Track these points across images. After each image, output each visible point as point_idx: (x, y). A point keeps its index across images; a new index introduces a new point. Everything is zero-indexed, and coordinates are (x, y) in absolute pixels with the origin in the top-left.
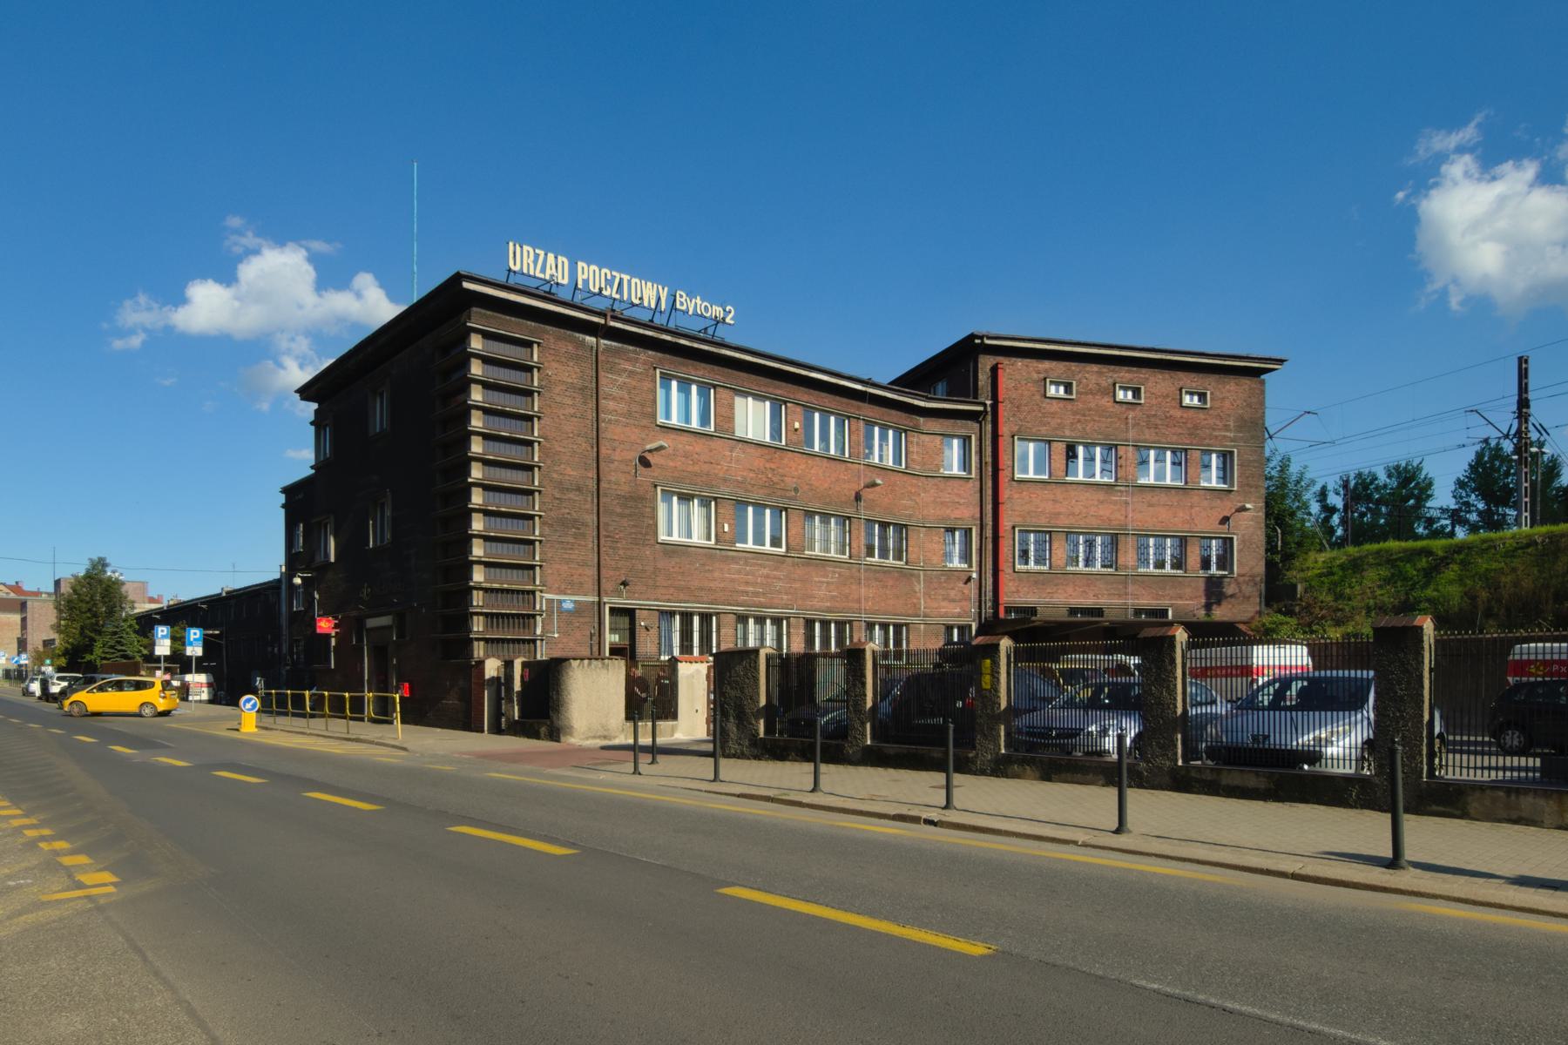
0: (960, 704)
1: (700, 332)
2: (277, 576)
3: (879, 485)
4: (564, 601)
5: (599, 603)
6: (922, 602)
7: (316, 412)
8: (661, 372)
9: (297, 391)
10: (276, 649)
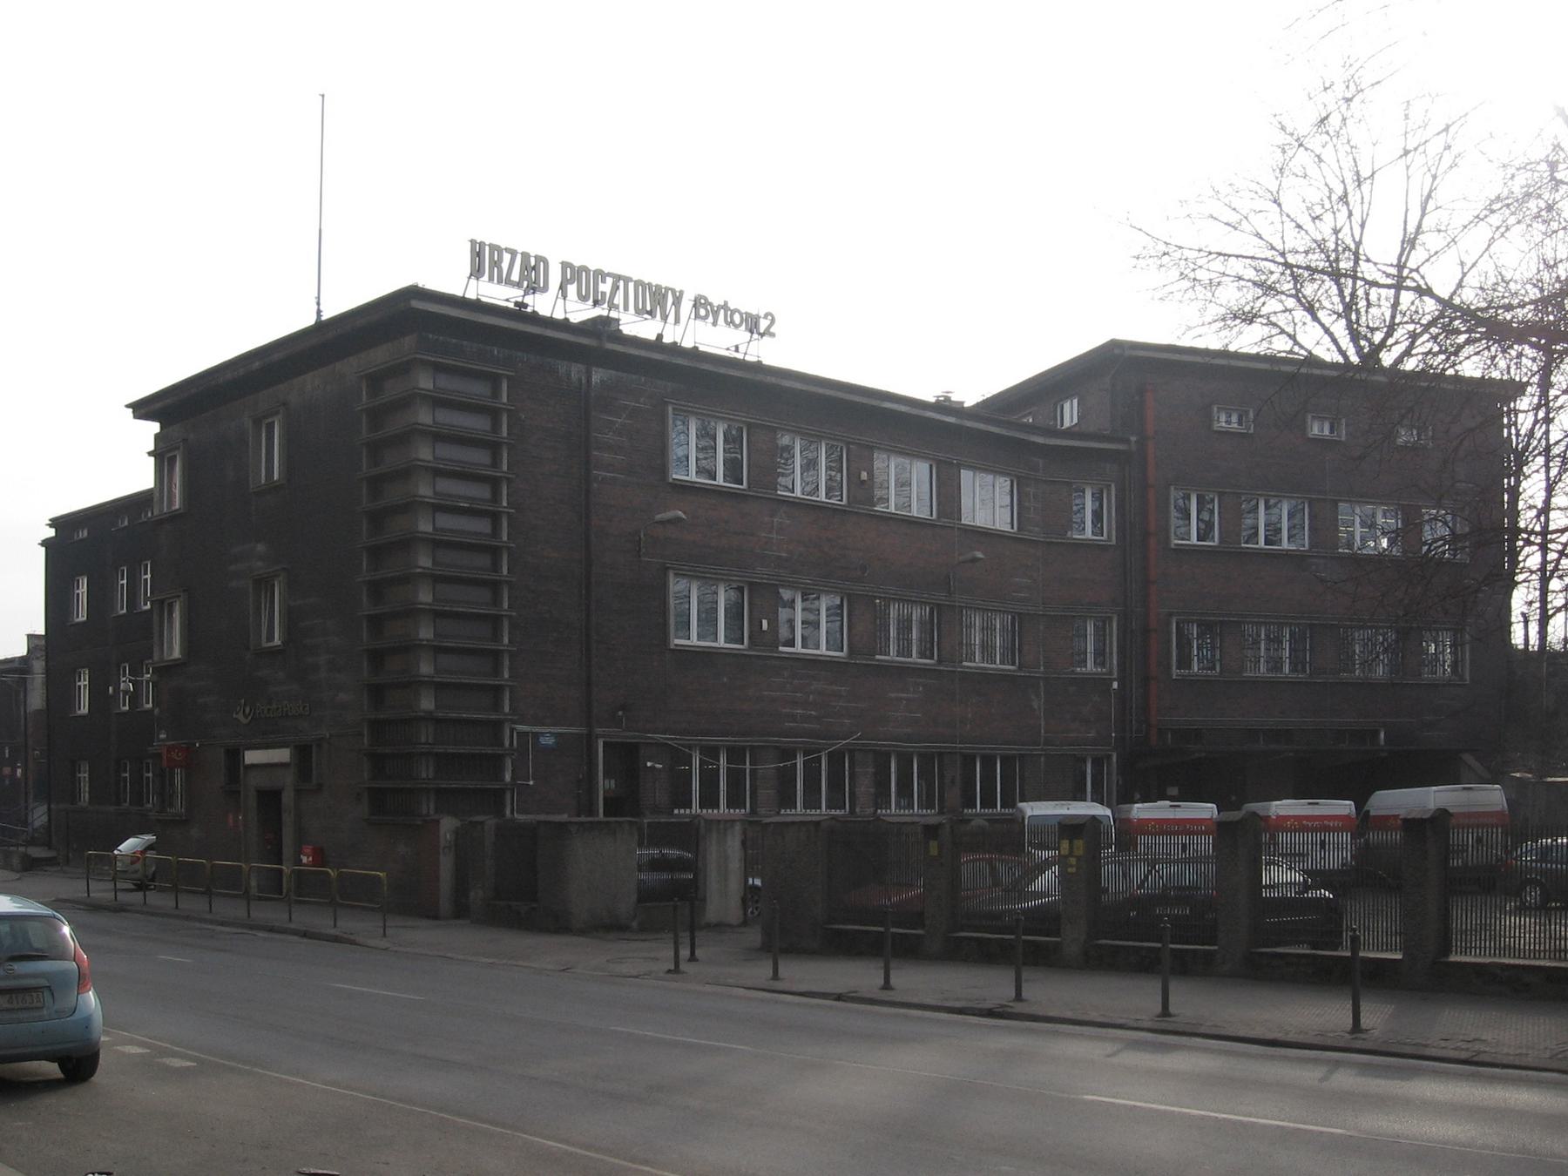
0: (1506, 537)
1: (728, 349)
2: (21, 650)
3: (980, 559)
4: (543, 734)
5: (589, 735)
6: (1043, 723)
7: (157, 437)
8: (674, 409)
9: (143, 409)
10: (19, 771)
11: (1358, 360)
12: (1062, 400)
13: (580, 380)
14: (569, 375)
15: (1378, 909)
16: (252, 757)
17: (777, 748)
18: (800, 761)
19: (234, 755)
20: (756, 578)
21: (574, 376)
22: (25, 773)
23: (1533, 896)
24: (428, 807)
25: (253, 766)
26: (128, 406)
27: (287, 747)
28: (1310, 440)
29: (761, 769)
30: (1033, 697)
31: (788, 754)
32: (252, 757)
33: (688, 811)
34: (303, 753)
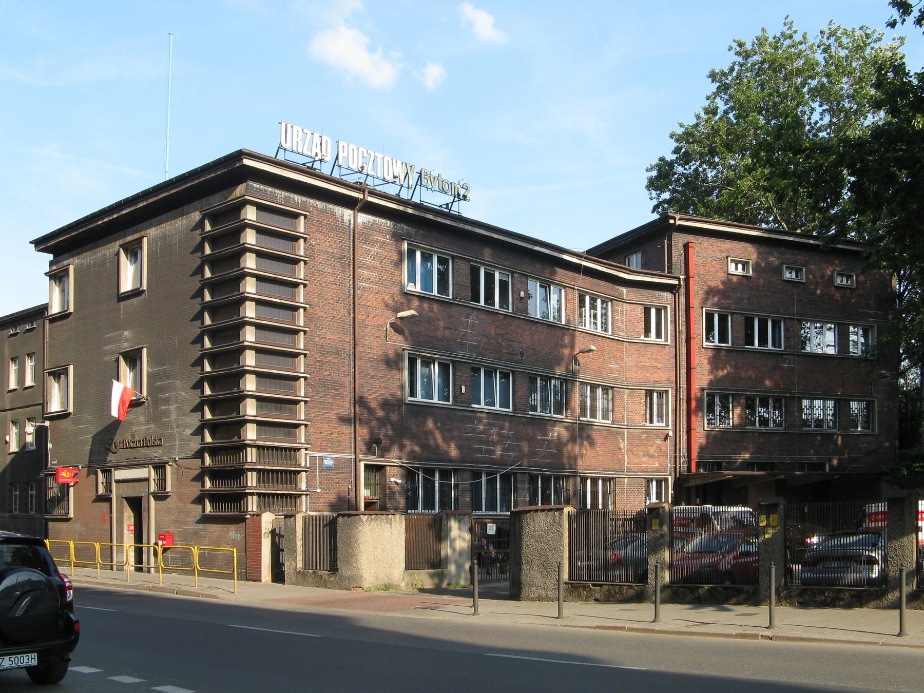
11: (536, 310)
12: (629, 255)
13: (350, 221)
14: (342, 217)
17: (471, 470)
18: (484, 479)
20: (458, 358)
21: (346, 218)
22: (837, 474)
24: (252, 504)
26: (31, 243)
28: (785, 281)
29: (461, 484)
30: (621, 441)
31: (477, 475)
33: (433, 511)
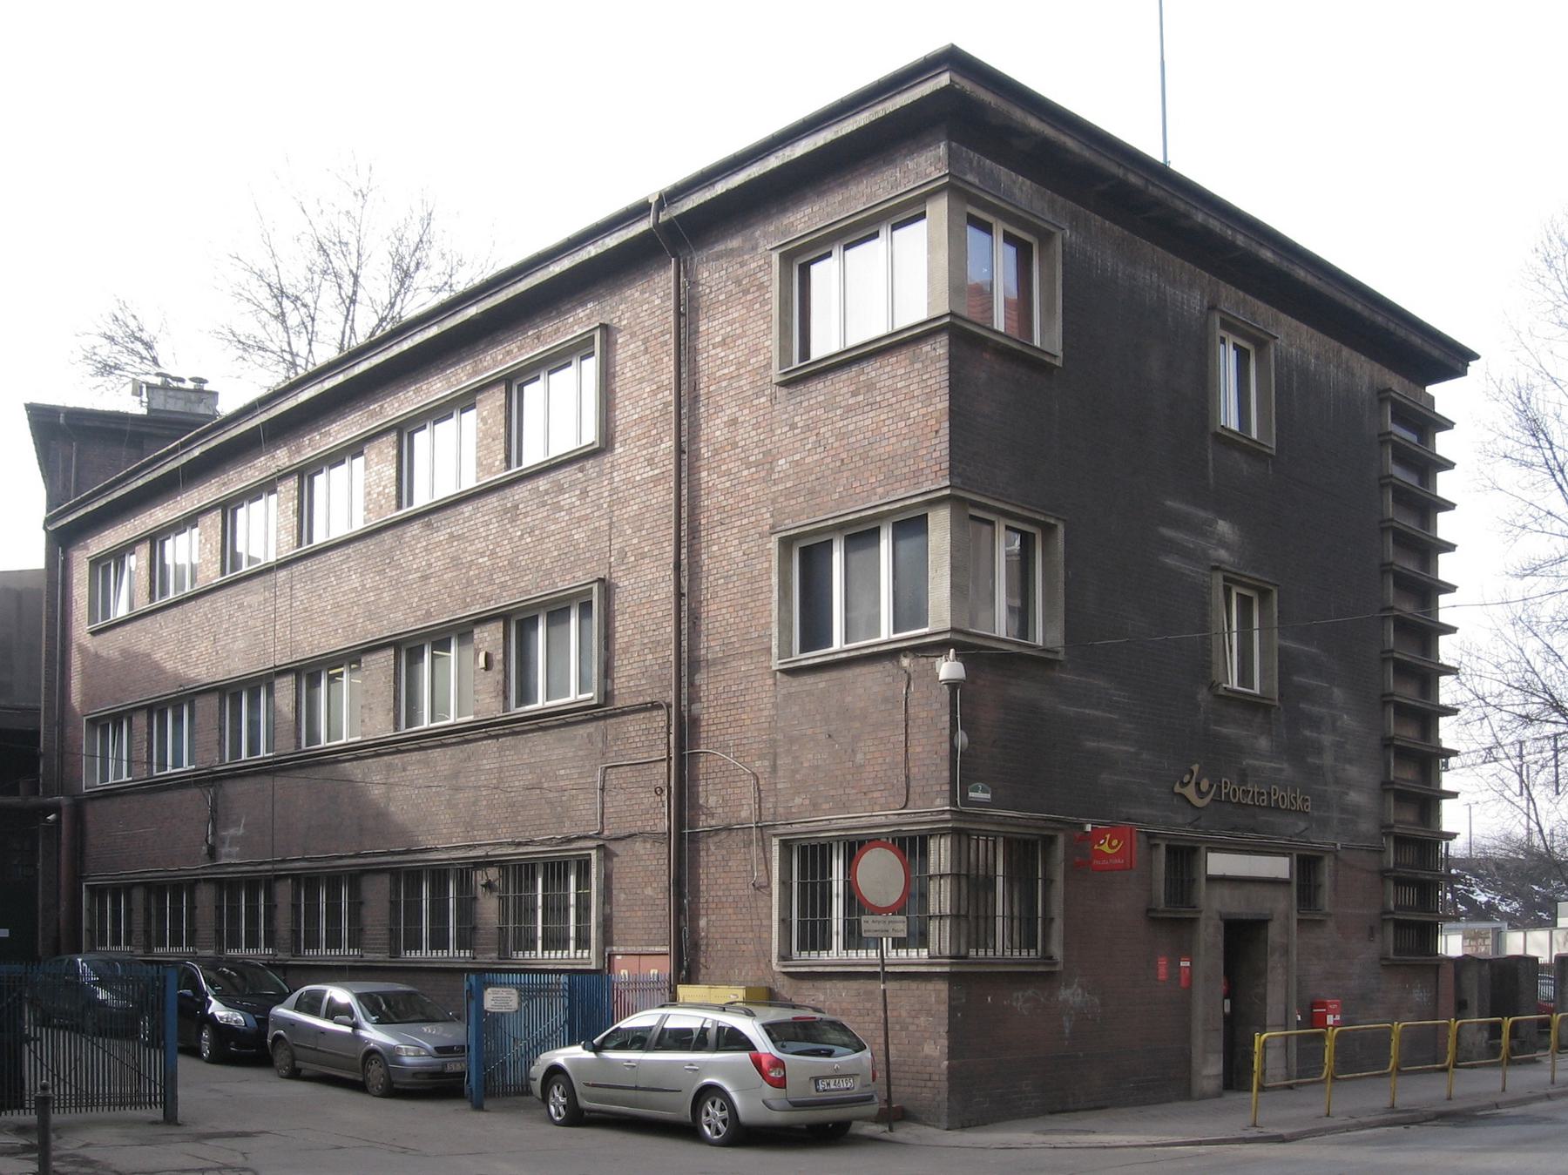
15: (377, 939)
16: (1219, 863)
19: (1183, 858)
23: (714, 1114)
25: (1214, 880)
27: (1284, 855)
32: (1219, 863)
34: (1307, 866)
